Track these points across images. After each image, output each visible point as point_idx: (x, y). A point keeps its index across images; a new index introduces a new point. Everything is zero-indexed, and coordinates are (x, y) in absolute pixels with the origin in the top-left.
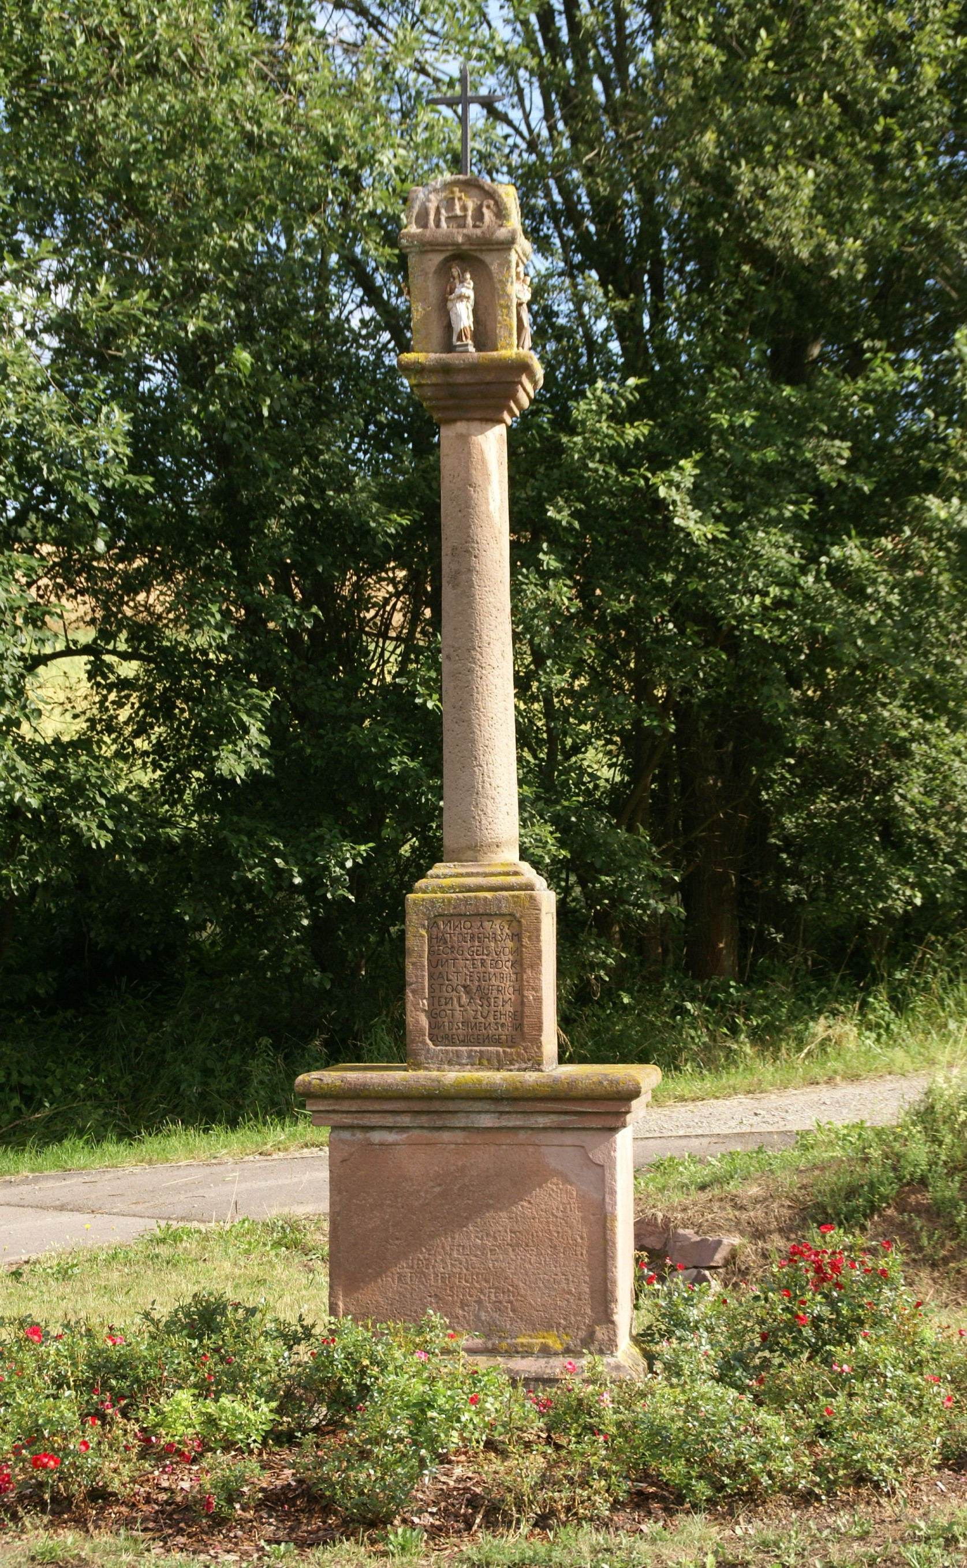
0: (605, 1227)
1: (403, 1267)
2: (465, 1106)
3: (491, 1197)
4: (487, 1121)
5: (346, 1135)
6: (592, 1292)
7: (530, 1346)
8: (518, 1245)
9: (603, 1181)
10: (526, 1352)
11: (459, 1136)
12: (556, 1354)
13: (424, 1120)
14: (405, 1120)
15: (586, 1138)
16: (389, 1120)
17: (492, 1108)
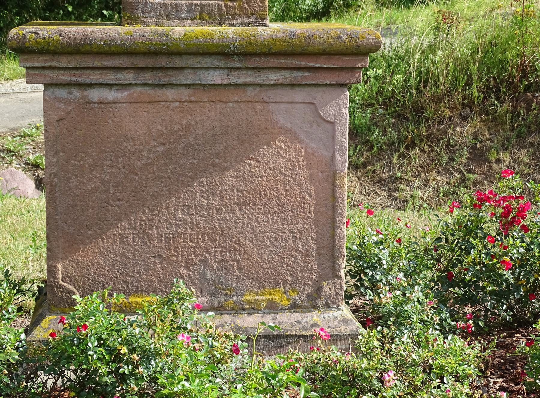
0: (334, 184)
1: (124, 227)
2: (193, 61)
3: (217, 155)
4: (215, 77)
5: (62, 93)
6: (319, 248)
7: (257, 303)
8: (245, 204)
9: (333, 138)
10: (253, 309)
11: (184, 94)
12: (283, 310)
13: (148, 77)
14: (128, 77)
15: (317, 95)
16: (111, 77)
17: (222, 64)
